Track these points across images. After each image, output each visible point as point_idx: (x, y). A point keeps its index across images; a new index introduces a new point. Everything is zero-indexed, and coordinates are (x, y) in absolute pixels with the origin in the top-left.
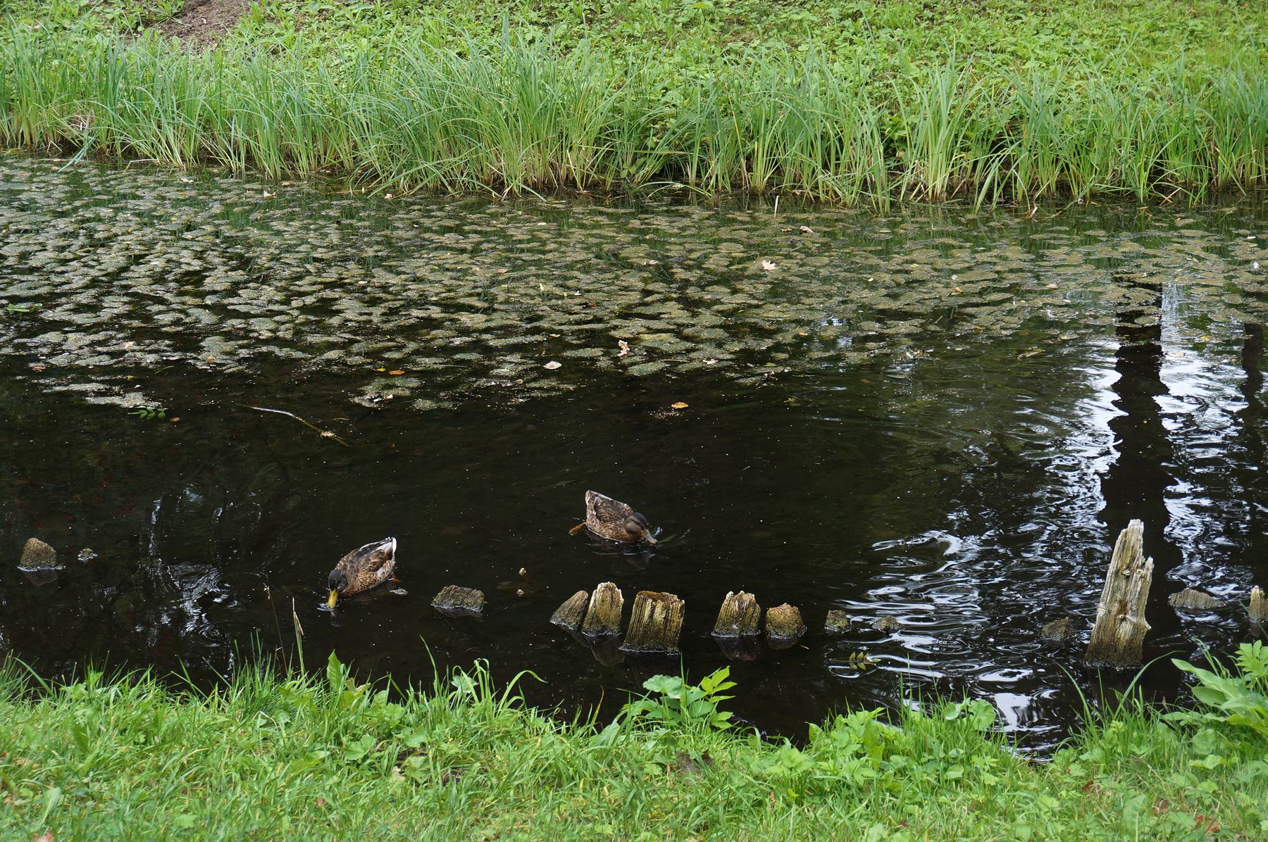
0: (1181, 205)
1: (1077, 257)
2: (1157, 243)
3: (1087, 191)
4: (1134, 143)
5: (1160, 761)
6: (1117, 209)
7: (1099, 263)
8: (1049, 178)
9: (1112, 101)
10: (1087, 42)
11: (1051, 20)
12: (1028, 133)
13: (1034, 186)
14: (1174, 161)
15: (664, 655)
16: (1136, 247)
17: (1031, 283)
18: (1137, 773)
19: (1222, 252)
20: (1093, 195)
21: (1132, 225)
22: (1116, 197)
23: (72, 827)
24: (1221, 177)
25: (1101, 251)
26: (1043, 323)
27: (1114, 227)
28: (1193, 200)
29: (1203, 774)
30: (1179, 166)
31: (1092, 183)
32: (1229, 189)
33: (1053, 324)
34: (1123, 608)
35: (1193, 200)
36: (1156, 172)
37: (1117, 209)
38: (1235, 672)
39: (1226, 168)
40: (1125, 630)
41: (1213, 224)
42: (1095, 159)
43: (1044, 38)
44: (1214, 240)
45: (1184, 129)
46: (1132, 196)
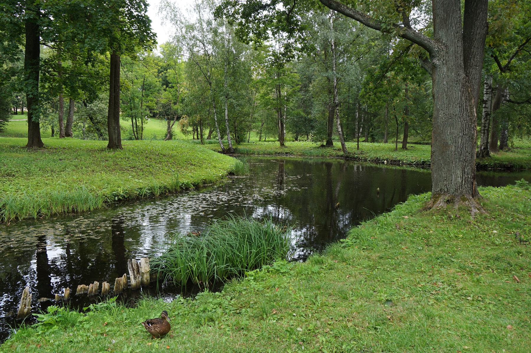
0: (44, 219)
1: (19, 233)
2: (39, 227)
3: (22, 218)
4: (33, 207)
5: (29, 336)
6: (30, 221)
7: (24, 233)
8: (13, 217)
9: (28, 198)
10: (22, 187)
11: (13, 183)
12: (7, 207)
13: (9, 218)
14: (43, 210)
15: (417, 6)
16: (34, 229)
17: (8, 240)
18: (21, 339)
19: (53, 227)
20: (24, 219)
21: (33, 224)
22: (30, 219)
23: (523, 93)
24: (53, 212)
25: (25, 231)
26: (10, 248)
27: (28, 225)
28: (47, 218)
29: (38, 335)
30: (44, 211)
31: (23, 216)
32: (55, 215)
33: (13, 248)
34: (25, 305)
35: (47, 218)
36: (39, 213)
37: (30, 221)
38: (47, 313)
39: (54, 210)
40: (26, 310)
41: (53, 222)
42: (24, 211)
43: (11, 187)
44: (51, 225)
45: (45, 203)
46: (33, 218)
